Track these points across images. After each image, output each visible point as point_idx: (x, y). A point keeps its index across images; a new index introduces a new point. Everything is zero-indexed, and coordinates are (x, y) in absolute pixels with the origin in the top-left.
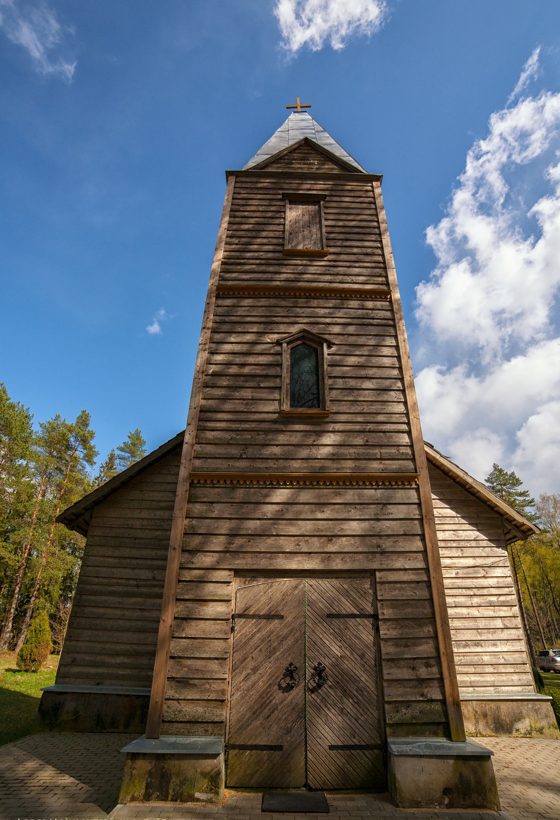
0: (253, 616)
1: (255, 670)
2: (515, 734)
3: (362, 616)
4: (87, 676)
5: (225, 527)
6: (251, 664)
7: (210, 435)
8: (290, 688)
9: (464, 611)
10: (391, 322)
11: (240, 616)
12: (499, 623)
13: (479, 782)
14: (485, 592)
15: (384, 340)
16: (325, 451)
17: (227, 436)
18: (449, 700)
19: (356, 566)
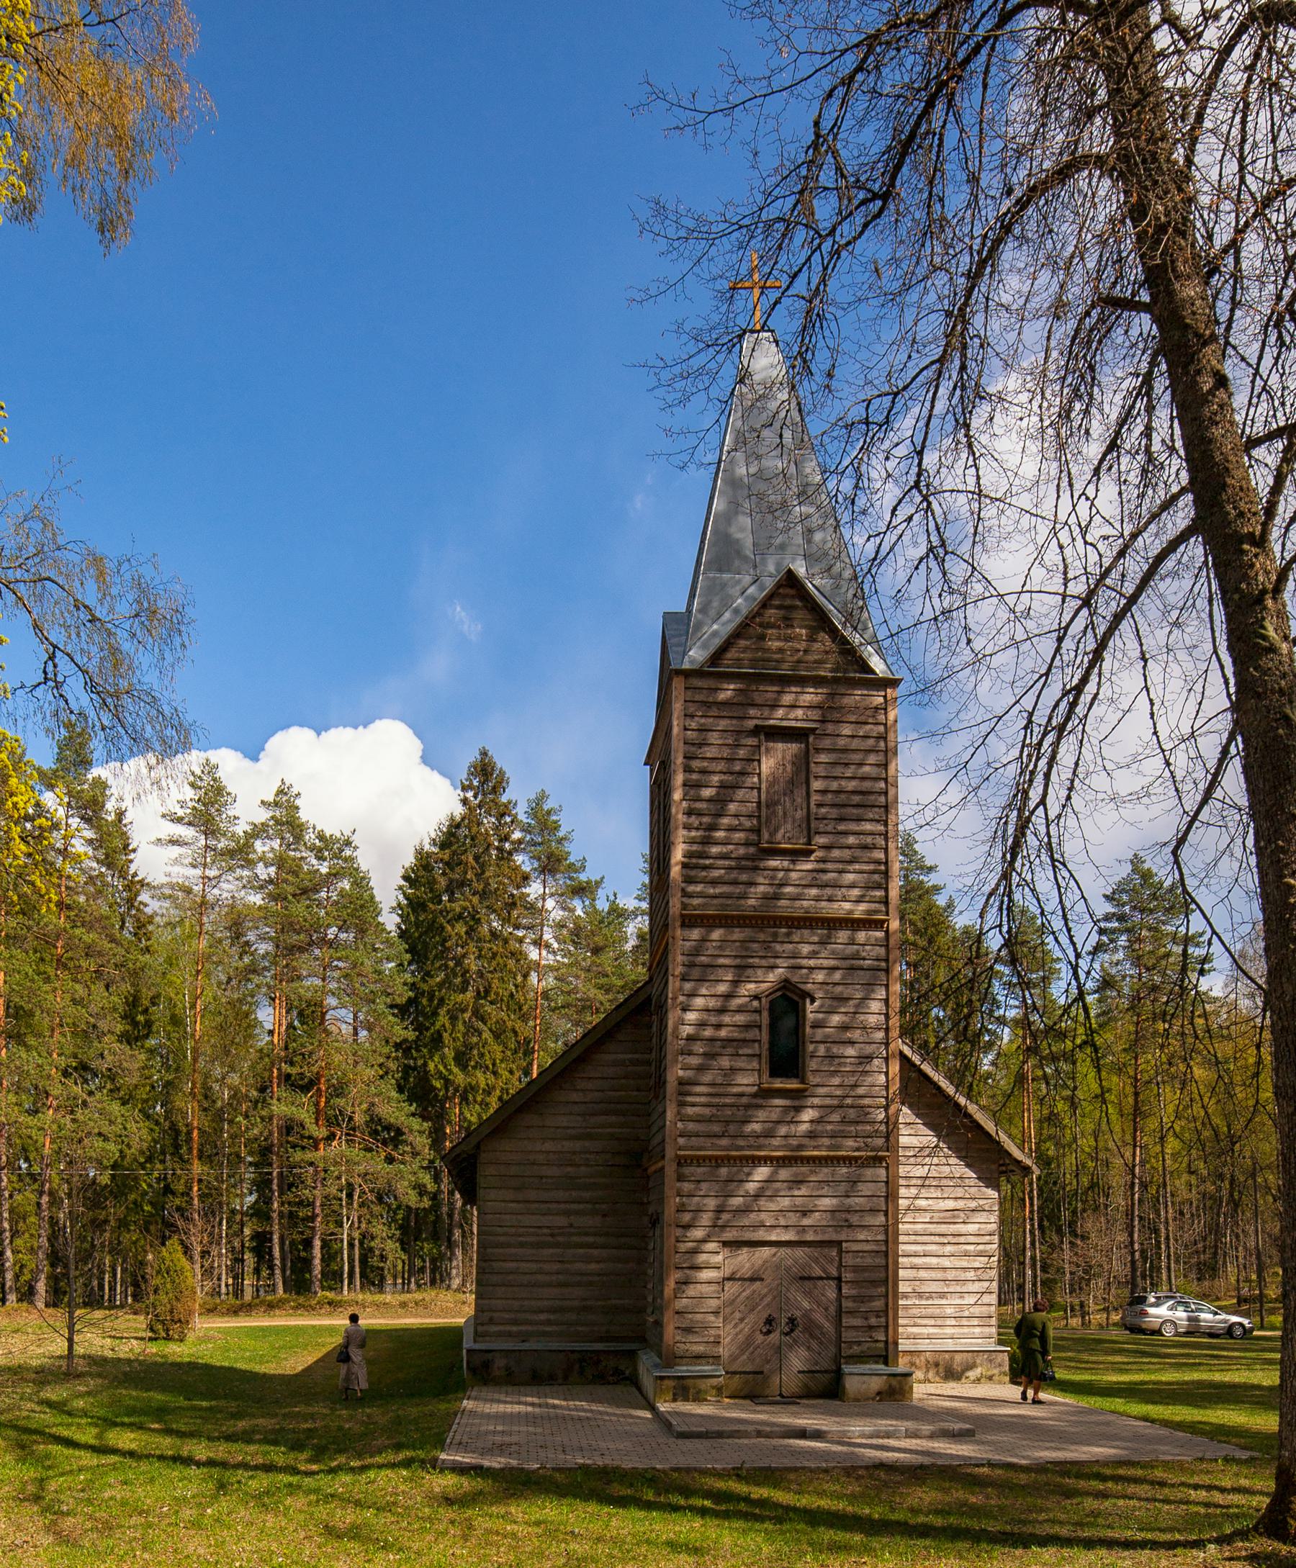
0: (739, 1279)
1: (742, 1320)
2: (963, 1380)
3: (828, 1278)
4: (510, 1334)
5: (711, 1203)
6: (738, 1315)
7: (690, 1111)
8: (769, 1332)
9: (934, 1261)
10: (883, 964)
11: (729, 1279)
12: (970, 1275)
13: (901, 1388)
14: (962, 1239)
15: (873, 991)
16: (804, 1128)
17: (707, 1111)
18: (890, 1340)
19: (826, 1237)
